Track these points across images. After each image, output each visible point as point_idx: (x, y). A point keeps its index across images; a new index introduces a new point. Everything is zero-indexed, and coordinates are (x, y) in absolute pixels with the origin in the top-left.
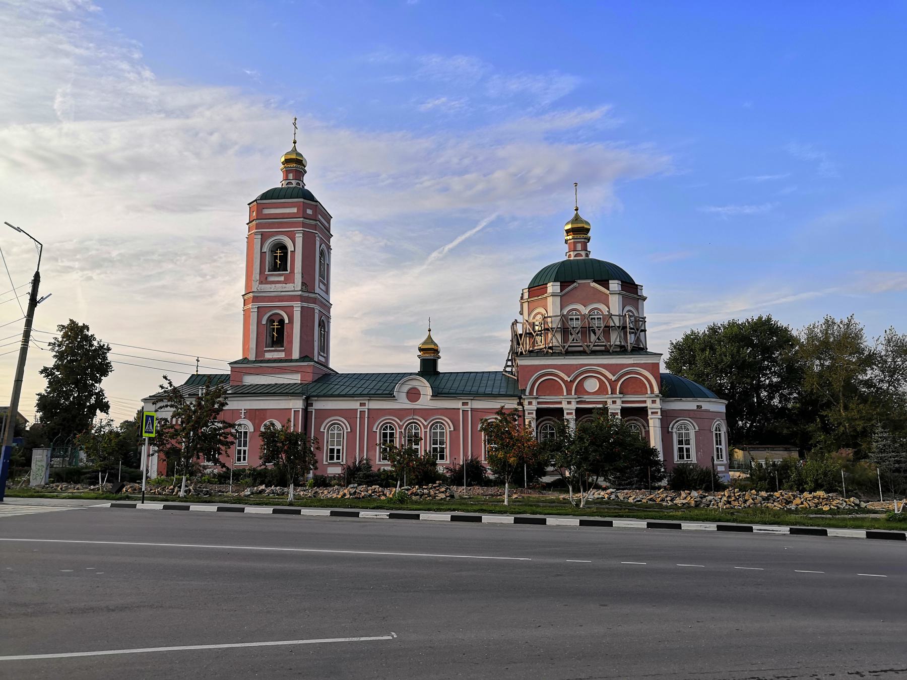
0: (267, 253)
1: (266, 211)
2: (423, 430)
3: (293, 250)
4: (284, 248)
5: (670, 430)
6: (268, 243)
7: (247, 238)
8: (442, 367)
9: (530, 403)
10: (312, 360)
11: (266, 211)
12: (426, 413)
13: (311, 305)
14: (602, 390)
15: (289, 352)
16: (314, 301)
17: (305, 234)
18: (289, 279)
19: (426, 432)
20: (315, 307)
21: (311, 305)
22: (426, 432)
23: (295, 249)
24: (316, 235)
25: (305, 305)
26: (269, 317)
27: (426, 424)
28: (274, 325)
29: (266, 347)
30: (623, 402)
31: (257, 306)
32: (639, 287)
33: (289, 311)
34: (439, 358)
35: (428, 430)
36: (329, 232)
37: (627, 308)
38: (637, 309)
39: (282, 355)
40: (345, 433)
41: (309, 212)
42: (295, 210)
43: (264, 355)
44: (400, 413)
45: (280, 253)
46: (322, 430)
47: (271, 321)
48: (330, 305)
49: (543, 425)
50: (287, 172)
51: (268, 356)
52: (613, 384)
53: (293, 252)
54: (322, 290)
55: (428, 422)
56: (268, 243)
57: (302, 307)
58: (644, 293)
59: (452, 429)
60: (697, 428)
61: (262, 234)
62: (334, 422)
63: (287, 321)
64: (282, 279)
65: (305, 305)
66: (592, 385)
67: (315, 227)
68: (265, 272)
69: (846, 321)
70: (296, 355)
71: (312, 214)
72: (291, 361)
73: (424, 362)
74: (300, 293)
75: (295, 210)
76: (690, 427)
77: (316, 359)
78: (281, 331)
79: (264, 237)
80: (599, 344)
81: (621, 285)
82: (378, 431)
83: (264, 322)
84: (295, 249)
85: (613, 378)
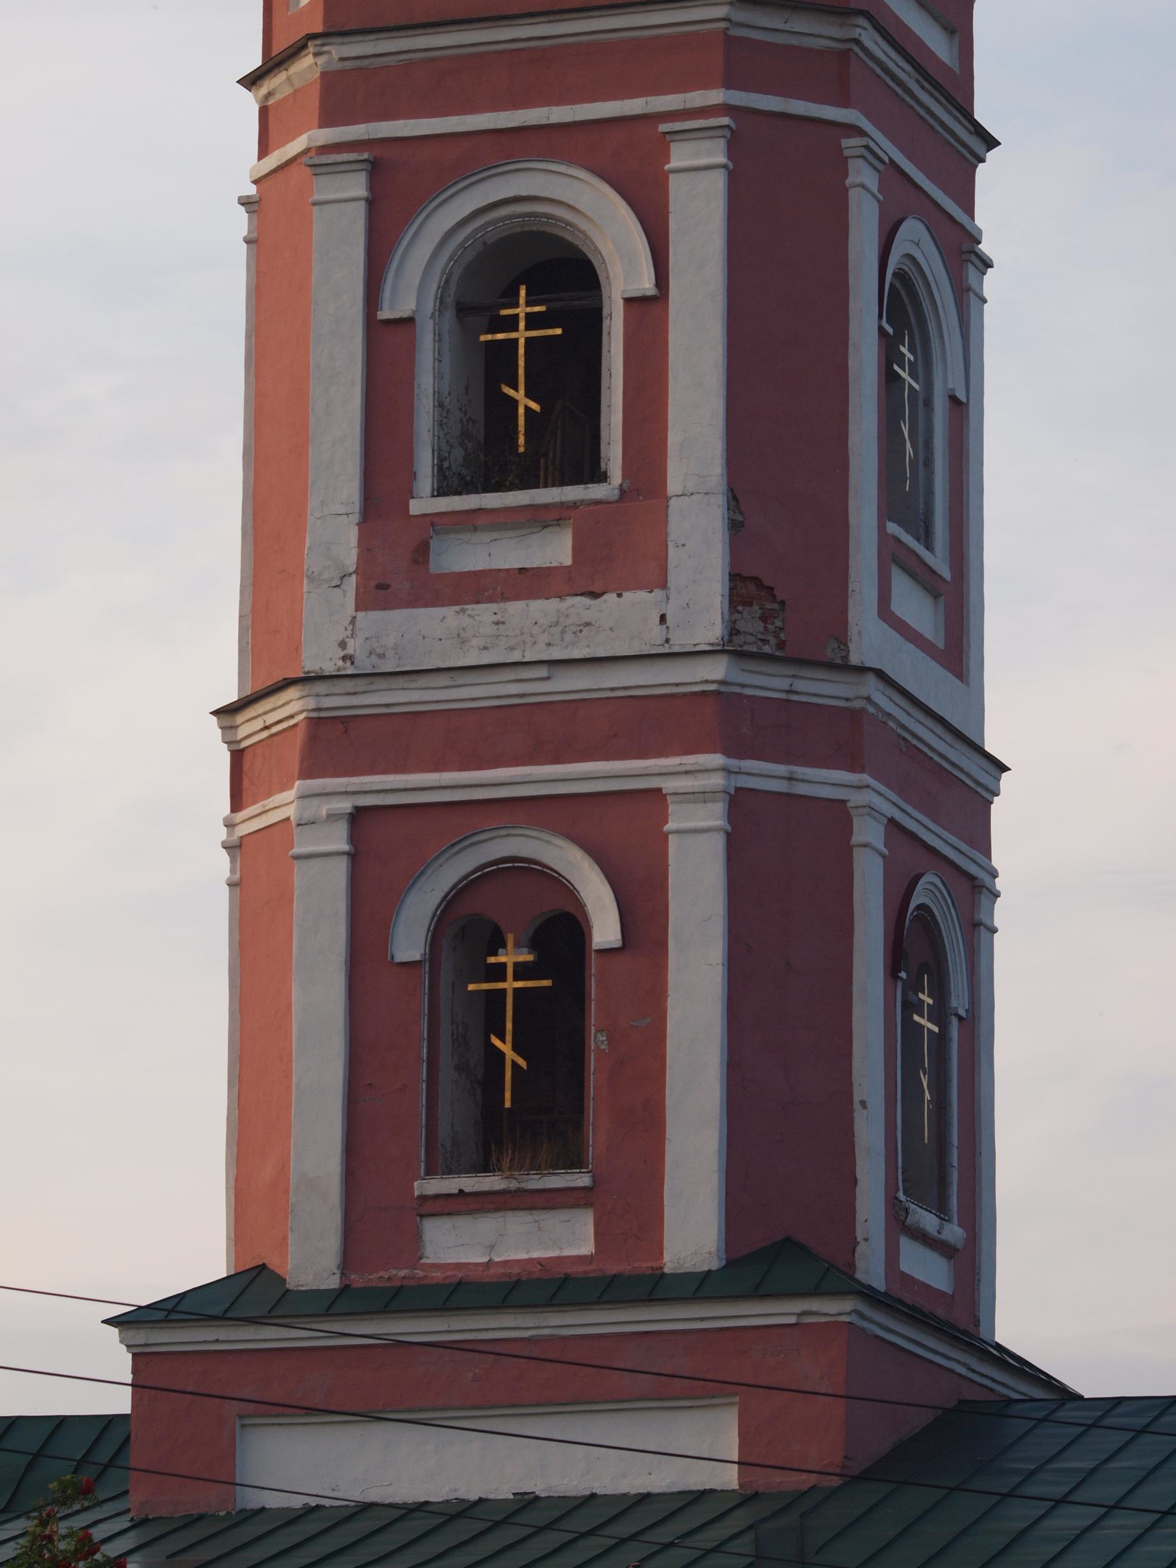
20: (856, 799)
24: (850, 144)
28: (498, 972)
29: (431, 1171)
31: (345, 805)
74: (716, 670)
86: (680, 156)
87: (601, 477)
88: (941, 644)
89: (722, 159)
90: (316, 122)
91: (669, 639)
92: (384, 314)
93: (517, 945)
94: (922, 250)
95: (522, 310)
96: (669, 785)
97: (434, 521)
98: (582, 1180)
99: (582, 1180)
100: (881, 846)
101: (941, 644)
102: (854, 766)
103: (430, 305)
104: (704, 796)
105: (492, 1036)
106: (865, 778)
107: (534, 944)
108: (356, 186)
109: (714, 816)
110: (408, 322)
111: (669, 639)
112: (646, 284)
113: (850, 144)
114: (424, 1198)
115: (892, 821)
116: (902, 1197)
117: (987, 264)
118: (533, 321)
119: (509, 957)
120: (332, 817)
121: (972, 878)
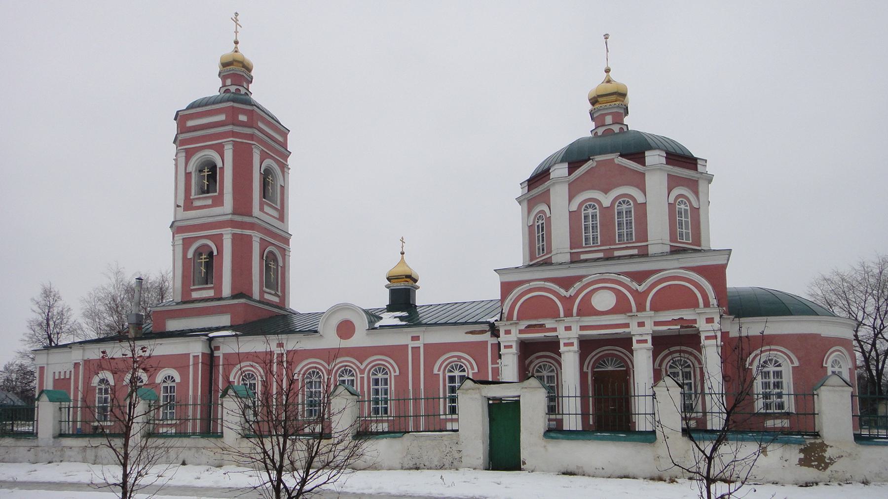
0: (193, 175)
1: (190, 123)
2: (359, 376)
3: (222, 166)
4: (213, 168)
5: (824, 365)
6: (192, 163)
7: (174, 159)
8: (421, 299)
9: (508, 332)
10: (250, 298)
11: (190, 123)
12: (361, 354)
13: (247, 232)
14: (621, 307)
15: (218, 288)
16: (252, 226)
17: (235, 144)
18: (218, 201)
19: (362, 378)
20: (252, 234)
21: (247, 232)
22: (362, 378)
23: (223, 165)
24: (253, 146)
25: (247, 219)
26: (198, 248)
27: (362, 367)
28: (202, 259)
29: (194, 285)
30: (656, 324)
31: (182, 237)
32: (699, 162)
33: (218, 239)
34: (418, 288)
35: (365, 376)
36: (287, 150)
37: (676, 192)
38: (696, 193)
39: (211, 293)
40: (393, 376)
41: (243, 118)
42: (222, 117)
43: (191, 294)
44: (331, 355)
45: (208, 172)
46: (436, 371)
47: (198, 253)
48: (287, 235)
49: (536, 365)
50: (223, 76)
51: (195, 295)
52: (640, 297)
53: (222, 169)
54: (274, 217)
55: (365, 363)
56: (192, 163)
57: (234, 235)
58: (710, 169)
59: (397, 373)
60: (796, 364)
61: (187, 151)
62: (315, 365)
63: (215, 253)
64: (209, 202)
65: (247, 219)
66: (604, 300)
67: (251, 137)
68: (191, 195)
69: (876, 271)
70: (226, 291)
71: (246, 120)
72: (221, 299)
73: (394, 293)
74: (229, 217)
75: (222, 117)
76: (782, 358)
77: (256, 295)
78: (209, 265)
79: (189, 154)
80: (629, 245)
81: (666, 158)
82: (441, 373)
83: (190, 255)
84: (223, 165)
85: (641, 289)
86: (226, 147)
87: (216, 192)
88: (278, 217)
89: (232, 147)
90: (502, 281)
91: (571, 330)
92: (187, 172)
93: (204, 255)
94: (645, 334)
95: (206, 170)
96: (223, 232)
97: (194, 199)
98: (212, 285)
99: (212, 285)
100: (259, 241)
101: (278, 217)
102: (253, 230)
103: (194, 170)
104: (228, 234)
105: (407, 314)
106: (254, 232)
107: (412, 306)
108: (184, 154)
109: (230, 236)
110: (191, 173)
111: (571, 330)
112: (222, 166)
113: (253, 146)
114: (192, 289)
115: (261, 238)
116: (264, 288)
117: (289, 169)
118: (208, 172)
119: (203, 257)
120: (180, 239)
121: (284, 249)
